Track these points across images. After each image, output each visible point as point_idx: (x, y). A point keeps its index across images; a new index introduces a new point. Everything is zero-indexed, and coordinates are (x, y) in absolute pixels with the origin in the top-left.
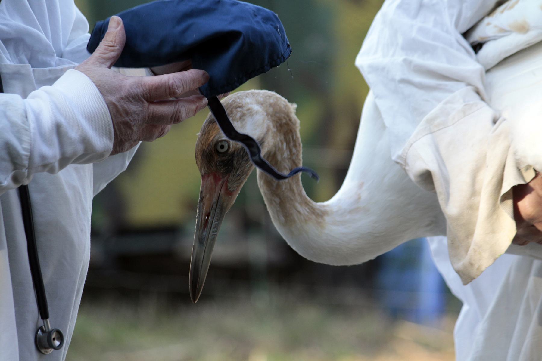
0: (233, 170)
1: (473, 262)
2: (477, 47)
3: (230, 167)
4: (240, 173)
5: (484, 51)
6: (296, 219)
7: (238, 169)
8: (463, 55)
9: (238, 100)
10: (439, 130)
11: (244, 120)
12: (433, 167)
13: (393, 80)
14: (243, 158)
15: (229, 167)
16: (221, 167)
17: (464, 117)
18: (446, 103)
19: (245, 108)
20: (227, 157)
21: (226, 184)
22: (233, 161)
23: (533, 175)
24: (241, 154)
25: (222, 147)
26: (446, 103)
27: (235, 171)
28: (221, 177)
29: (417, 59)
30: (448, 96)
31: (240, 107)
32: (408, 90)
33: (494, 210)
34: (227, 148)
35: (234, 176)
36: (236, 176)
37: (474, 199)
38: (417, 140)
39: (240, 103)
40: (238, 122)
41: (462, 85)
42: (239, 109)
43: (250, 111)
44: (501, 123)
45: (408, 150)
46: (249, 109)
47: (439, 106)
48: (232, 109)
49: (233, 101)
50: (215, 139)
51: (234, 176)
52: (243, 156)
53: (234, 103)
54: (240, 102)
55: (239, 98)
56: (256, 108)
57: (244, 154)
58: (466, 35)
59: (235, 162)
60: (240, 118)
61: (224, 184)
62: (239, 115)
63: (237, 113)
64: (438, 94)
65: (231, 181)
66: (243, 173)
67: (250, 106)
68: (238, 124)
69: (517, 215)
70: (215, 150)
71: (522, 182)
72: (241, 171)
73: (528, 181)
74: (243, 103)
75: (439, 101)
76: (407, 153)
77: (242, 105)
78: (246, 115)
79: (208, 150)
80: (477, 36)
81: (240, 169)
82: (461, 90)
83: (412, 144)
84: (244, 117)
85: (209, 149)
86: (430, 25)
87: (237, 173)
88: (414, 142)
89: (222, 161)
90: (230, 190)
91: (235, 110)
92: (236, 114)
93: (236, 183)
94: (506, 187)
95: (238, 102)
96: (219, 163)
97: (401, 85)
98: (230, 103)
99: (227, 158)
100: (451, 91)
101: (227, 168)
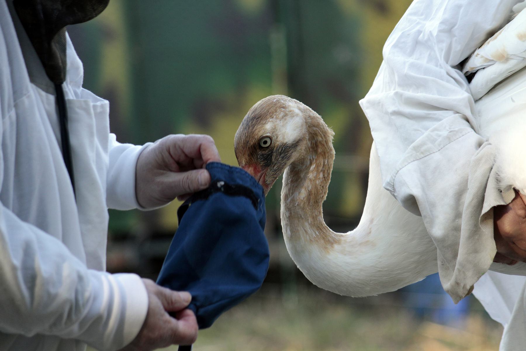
0: (271, 164)
1: (459, 282)
2: (470, 77)
3: (269, 162)
4: (276, 169)
5: (476, 80)
6: (301, 236)
7: (276, 164)
8: (453, 86)
9: (282, 101)
10: (425, 156)
11: (285, 119)
12: (416, 192)
13: (387, 113)
14: (280, 155)
15: (268, 161)
16: (261, 160)
17: (450, 143)
18: (433, 131)
19: (287, 110)
20: (267, 151)
21: (264, 176)
22: (271, 156)
23: (513, 195)
24: (280, 151)
25: (265, 142)
26: (433, 131)
27: (273, 166)
28: (260, 169)
29: (410, 93)
30: (436, 124)
31: (283, 108)
32: (399, 121)
33: (475, 231)
34: (269, 145)
35: (271, 170)
36: (273, 170)
37: (458, 221)
38: (403, 167)
39: (283, 104)
40: (280, 120)
41: (451, 113)
42: (283, 109)
43: (291, 113)
44: (484, 147)
45: (395, 177)
46: (291, 111)
47: (426, 133)
48: (276, 108)
49: (277, 101)
50: (260, 133)
51: (271, 170)
52: (280, 153)
53: (279, 103)
54: (284, 103)
55: (283, 100)
56: (297, 111)
57: (282, 152)
58: (461, 66)
59: (273, 158)
60: (283, 118)
61: (262, 177)
62: (282, 114)
63: (281, 112)
64: (426, 123)
65: (269, 174)
66: (278, 169)
67: (292, 109)
68: (280, 123)
69: (498, 235)
70: (258, 144)
71: (502, 203)
72: (277, 167)
73: (508, 203)
74: (287, 105)
75: (426, 129)
76: (394, 180)
77: (286, 106)
78: (287, 116)
79: (252, 143)
80: (469, 67)
81: (276, 165)
82: (448, 118)
83: (398, 171)
84: (287, 117)
85: (253, 142)
86: (424, 62)
87: (274, 168)
88: (401, 169)
89: (263, 155)
90: (267, 182)
91: (279, 109)
92: (280, 113)
93: (272, 177)
94: (486, 208)
95: (281, 102)
96: (260, 156)
97: (393, 117)
98: (275, 102)
99: (267, 153)
100: (438, 120)
101: (266, 162)
